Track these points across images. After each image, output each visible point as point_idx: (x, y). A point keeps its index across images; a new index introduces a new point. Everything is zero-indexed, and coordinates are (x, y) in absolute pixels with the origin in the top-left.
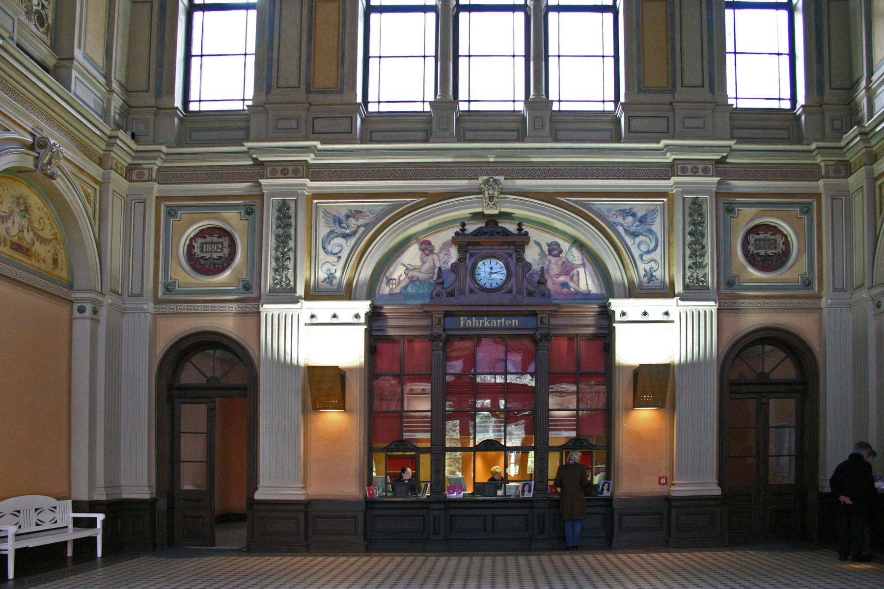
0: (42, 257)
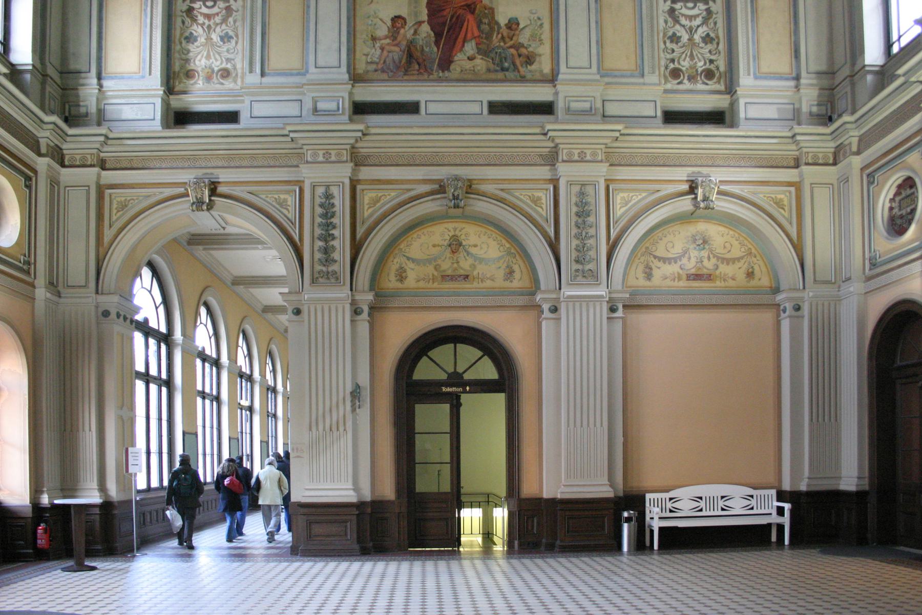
0: (730, 275)
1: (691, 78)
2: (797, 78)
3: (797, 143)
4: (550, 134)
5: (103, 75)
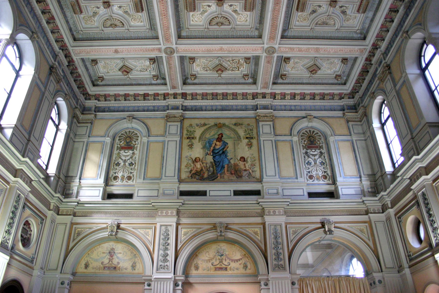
1: (318, 179)
2: (360, 177)
3: (364, 203)
4: (260, 203)
5: (82, 178)
